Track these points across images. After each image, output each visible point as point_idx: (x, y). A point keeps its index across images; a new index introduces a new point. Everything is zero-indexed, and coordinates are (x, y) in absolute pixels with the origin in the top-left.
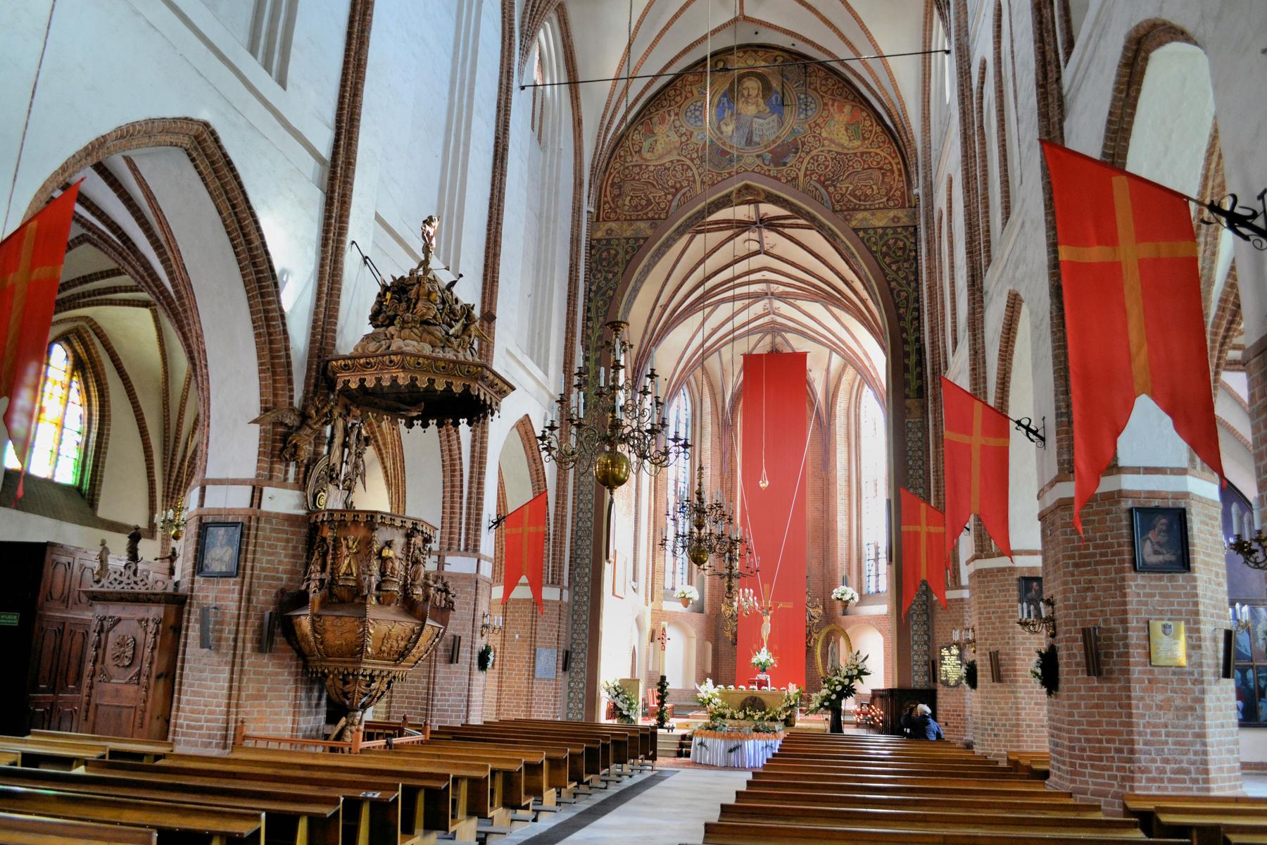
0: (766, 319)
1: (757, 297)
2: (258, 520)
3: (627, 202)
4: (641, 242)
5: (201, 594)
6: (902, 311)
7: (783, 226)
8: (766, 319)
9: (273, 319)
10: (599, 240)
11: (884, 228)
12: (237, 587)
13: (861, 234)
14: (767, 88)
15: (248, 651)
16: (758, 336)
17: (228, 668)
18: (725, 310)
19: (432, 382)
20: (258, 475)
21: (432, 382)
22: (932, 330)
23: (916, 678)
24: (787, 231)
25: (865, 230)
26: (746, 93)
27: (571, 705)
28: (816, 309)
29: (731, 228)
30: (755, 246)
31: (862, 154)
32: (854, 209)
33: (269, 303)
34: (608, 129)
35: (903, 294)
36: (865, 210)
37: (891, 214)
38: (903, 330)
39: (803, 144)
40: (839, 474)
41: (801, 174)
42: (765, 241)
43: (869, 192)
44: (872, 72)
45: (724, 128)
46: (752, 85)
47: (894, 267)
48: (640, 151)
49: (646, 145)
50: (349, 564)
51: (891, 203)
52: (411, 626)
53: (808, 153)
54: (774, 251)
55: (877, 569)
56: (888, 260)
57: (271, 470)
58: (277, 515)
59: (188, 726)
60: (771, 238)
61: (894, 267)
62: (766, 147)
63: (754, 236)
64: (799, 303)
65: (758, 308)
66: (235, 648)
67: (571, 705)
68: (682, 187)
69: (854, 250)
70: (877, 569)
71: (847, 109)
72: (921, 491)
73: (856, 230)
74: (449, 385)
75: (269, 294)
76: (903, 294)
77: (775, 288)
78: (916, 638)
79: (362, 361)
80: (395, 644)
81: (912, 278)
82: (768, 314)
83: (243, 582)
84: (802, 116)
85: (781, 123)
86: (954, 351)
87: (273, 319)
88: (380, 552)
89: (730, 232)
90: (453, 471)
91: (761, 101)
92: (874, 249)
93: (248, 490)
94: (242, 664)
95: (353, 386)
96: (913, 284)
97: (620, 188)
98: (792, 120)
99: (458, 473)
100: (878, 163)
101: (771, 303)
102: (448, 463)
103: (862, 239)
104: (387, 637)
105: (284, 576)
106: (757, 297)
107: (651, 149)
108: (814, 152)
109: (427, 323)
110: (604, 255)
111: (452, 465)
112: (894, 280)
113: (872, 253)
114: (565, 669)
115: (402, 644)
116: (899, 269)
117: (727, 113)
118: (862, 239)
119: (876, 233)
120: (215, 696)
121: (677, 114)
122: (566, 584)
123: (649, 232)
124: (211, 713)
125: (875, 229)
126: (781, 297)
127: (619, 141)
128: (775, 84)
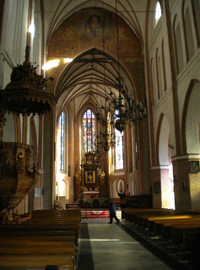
0: (88, 90)
1: (87, 83)
3: (58, 51)
6: (140, 87)
7: (100, 61)
8: (88, 90)
11: (135, 63)
14: (99, 20)
16: (86, 95)
18: (78, 87)
19: (36, 99)
21: (36, 99)
22: (149, 93)
25: (129, 63)
26: (93, 21)
27: (45, 205)
29: (81, 62)
30: (90, 67)
31: (128, 41)
32: (126, 57)
34: (52, 28)
35: (140, 82)
36: (129, 57)
37: (136, 59)
38: (141, 92)
39: (111, 37)
41: (110, 46)
43: (130, 52)
44: (130, 16)
45: (87, 31)
46: (95, 19)
47: (137, 74)
48: (62, 36)
49: (63, 35)
51: (136, 56)
52: (30, 181)
53: (112, 40)
56: (135, 72)
60: (96, 65)
61: (137, 74)
62: (100, 37)
64: (100, 85)
65: (87, 86)
67: (45, 205)
68: (75, 48)
69: (126, 69)
71: (123, 28)
72: (146, 138)
73: (126, 63)
74: (42, 100)
76: (140, 82)
77: (93, 80)
78: (146, 180)
79: (13, 92)
80: (25, 187)
82: (90, 88)
84: (110, 29)
85: (104, 31)
86: (159, 98)
89: (83, 63)
91: (98, 23)
92: (132, 68)
96: (143, 79)
97: (56, 47)
98: (107, 30)
99: (19, 133)
100: (132, 44)
101: (91, 85)
102: (16, 129)
104: (23, 184)
106: (87, 83)
107: (65, 36)
108: (114, 40)
109: (31, 80)
111: (18, 130)
112: (137, 78)
113: (131, 70)
114: (42, 194)
115: (28, 186)
116: (139, 75)
117: (88, 26)
121: (72, 26)
122: (42, 168)
125: (131, 63)
127: (55, 32)
128: (102, 19)
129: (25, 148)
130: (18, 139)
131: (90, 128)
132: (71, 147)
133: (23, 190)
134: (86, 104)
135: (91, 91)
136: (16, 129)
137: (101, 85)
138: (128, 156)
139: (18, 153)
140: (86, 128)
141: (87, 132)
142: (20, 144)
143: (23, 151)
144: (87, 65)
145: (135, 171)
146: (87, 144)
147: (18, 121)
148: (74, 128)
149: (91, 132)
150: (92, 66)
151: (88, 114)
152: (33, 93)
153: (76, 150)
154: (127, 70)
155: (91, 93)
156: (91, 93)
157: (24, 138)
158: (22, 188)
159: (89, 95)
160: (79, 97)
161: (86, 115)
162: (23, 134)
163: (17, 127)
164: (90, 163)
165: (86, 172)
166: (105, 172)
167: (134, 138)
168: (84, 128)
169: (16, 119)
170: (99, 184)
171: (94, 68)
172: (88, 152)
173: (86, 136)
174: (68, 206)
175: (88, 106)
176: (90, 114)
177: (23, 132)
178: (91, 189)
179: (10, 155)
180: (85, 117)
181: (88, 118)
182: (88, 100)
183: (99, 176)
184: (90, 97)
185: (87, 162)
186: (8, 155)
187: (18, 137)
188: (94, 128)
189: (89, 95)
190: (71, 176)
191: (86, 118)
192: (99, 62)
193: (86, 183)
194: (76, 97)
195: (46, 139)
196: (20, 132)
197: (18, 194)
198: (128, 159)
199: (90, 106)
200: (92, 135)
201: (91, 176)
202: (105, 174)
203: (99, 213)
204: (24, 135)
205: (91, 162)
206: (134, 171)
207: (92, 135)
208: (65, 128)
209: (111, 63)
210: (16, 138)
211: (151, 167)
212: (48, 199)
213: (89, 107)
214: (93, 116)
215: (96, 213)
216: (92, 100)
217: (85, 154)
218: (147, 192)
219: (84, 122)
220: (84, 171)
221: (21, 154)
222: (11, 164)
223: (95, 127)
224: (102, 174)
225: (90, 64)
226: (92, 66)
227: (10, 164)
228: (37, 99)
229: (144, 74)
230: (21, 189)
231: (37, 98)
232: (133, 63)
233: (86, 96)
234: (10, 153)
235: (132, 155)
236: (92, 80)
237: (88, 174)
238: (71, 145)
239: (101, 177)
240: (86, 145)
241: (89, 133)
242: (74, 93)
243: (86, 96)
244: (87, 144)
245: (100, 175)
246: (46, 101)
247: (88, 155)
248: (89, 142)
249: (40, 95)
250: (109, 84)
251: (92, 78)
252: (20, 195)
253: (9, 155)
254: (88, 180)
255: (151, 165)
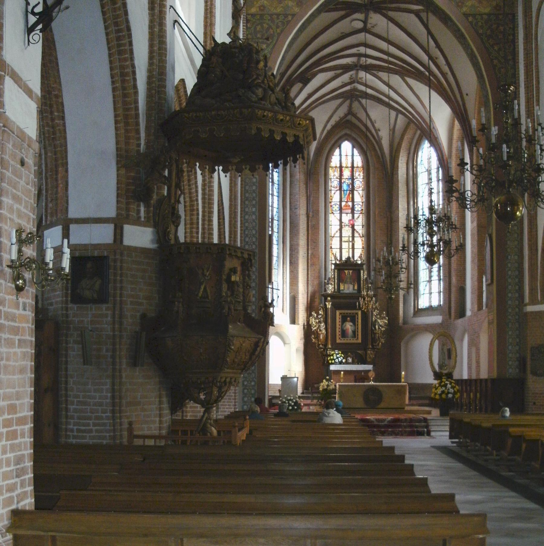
0: (348, 88)
1: (346, 68)
2: (122, 254)
4: (290, 18)
5: (76, 319)
8: (348, 88)
9: (127, 74)
10: (253, 15)
12: (109, 312)
13: (470, 19)
15: (124, 366)
16: (340, 101)
17: (108, 381)
20: (118, 215)
23: (510, 370)
24: (390, 13)
25: (474, 16)
27: (246, 399)
28: (396, 80)
30: (360, 25)
33: (125, 60)
40: (400, 215)
42: (370, 21)
47: (496, 48)
50: (205, 288)
54: (374, 30)
55: (430, 289)
57: (128, 210)
58: (136, 249)
59: (78, 431)
61: (496, 48)
63: (361, 16)
64: (381, 74)
65: (346, 78)
66: (114, 363)
67: (246, 399)
70: (430, 289)
73: (466, 15)
75: (125, 52)
81: (510, 57)
83: (114, 308)
87: (127, 74)
88: (229, 277)
89: (342, 13)
90: (192, 210)
92: (481, 31)
93: (111, 227)
94: (121, 377)
95: (278, 137)
96: (511, 63)
101: (357, 74)
103: (471, 23)
105: (144, 301)
106: (346, 68)
110: (258, 28)
111: (192, 206)
118: (471, 23)
119: (482, 18)
120: (101, 404)
123: (296, 10)
124: (97, 418)
125: (481, 15)
126: (368, 68)
129: (243, 257)
130: (192, 228)
131: (348, 192)
132: (298, 245)
133: (238, 365)
134: (337, 126)
135: (355, 89)
136: (188, 204)
137: (384, 75)
138: (453, 273)
139: (226, 270)
140: (338, 192)
141: (341, 205)
142: (231, 248)
143: (235, 263)
144: (348, 19)
145: (474, 315)
146: (341, 237)
147: (193, 182)
148: (307, 192)
149: (350, 204)
150: (365, 22)
151: (343, 154)
152: (264, 116)
153: (312, 254)
154: (467, 36)
155: (352, 95)
156: (352, 95)
157: (206, 226)
158: (236, 360)
159: (348, 102)
160: (323, 106)
161: (338, 157)
162: (203, 216)
163: (190, 198)
164: (349, 288)
165: (338, 312)
166: (388, 315)
167: (475, 224)
168: (333, 192)
169: (189, 176)
170: (373, 346)
171: (369, 26)
172: (344, 259)
173: (338, 216)
174: (274, 401)
175: (343, 133)
176: (350, 154)
177: (204, 212)
178: (350, 360)
179: (207, 274)
180: (335, 161)
181: (344, 165)
182: (346, 115)
183: (374, 324)
184: (350, 107)
185: (342, 287)
186: (204, 275)
187: (192, 224)
188: (361, 192)
189: (348, 102)
190: (299, 324)
191: (338, 165)
192: (385, 12)
193: (338, 341)
194: (313, 109)
195: (247, 224)
196: (198, 210)
197: (227, 374)
198: (454, 280)
199: (348, 132)
200: (353, 213)
201: (351, 324)
202: (388, 320)
203: (386, 423)
204: (207, 218)
205: (351, 287)
206: (469, 313)
207: (353, 213)
208: (281, 191)
209: (417, 14)
210: (188, 226)
211: (526, 305)
212: (253, 383)
213: (346, 134)
214: (358, 161)
215: (376, 423)
216: (355, 116)
217: (336, 264)
218: (512, 371)
219: (333, 174)
220: (332, 312)
221: (233, 271)
222: (210, 298)
223: (362, 190)
224: (382, 318)
225: (357, 16)
226: (365, 22)
227: (208, 297)
228: (273, 131)
229: (514, 48)
230: (234, 361)
231: (273, 128)
232: (485, 17)
233: (340, 105)
234: (207, 271)
235: (464, 269)
236: (359, 60)
237: (344, 319)
238: (298, 239)
239: (377, 327)
240: (338, 239)
241: (346, 206)
242: (310, 96)
243: (340, 105)
244: (341, 237)
245: (376, 320)
246: (295, 136)
247: (345, 267)
248: (347, 232)
249: (282, 120)
250: (408, 70)
251: (359, 55)
252: (232, 375)
253: (205, 275)
254: (344, 334)
255: (527, 300)
